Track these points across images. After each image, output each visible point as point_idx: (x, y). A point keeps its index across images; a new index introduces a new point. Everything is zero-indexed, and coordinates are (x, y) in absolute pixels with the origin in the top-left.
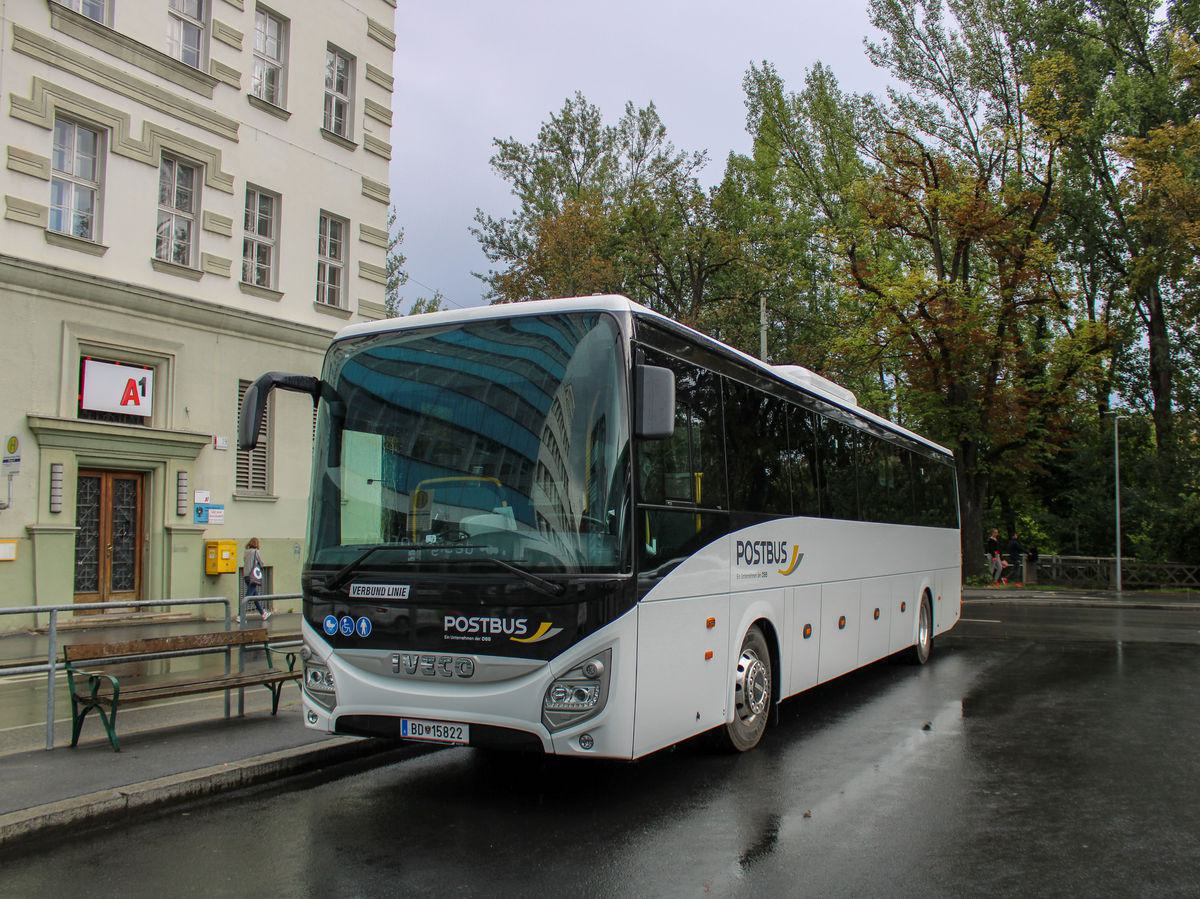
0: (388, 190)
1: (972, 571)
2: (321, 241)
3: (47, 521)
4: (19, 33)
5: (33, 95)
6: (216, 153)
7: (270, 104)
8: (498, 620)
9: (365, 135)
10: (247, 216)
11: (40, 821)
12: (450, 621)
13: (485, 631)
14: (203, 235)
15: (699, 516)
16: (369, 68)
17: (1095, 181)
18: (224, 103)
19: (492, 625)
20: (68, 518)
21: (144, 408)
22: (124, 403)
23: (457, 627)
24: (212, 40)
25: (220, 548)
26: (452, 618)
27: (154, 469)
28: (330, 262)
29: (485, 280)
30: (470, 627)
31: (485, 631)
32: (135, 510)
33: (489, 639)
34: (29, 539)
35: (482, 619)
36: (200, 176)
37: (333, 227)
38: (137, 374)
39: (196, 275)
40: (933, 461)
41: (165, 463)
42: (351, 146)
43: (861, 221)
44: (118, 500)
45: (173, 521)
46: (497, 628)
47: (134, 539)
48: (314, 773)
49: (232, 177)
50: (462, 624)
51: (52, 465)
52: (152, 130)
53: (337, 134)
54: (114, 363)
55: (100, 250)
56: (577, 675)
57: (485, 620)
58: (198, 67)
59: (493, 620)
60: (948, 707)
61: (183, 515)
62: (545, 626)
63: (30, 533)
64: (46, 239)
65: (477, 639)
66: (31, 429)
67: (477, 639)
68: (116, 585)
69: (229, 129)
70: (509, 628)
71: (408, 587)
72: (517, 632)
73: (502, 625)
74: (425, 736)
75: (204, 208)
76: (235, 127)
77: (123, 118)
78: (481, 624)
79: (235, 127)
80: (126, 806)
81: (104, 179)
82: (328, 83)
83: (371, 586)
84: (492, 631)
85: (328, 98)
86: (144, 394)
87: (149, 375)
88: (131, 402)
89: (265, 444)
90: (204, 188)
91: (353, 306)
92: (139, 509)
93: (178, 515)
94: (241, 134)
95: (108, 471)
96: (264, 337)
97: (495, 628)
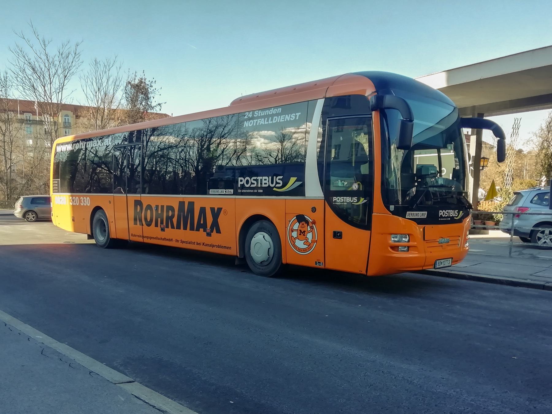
1: (304, 125)
8: (267, 178)
12: (335, 199)
13: (345, 201)
15: (330, 128)
19: (264, 182)
23: (337, 200)
26: (242, 178)
30: (252, 183)
31: (345, 201)
33: (346, 204)
35: (344, 198)
40: (421, 191)
46: (348, 200)
48: (446, 219)
50: (247, 182)
57: (345, 198)
60: (232, 173)
65: (343, 204)
67: (343, 204)
70: (352, 200)
72: (354, 201)
73: (350, 199)
78: (344, 199)
84: (347, 201)
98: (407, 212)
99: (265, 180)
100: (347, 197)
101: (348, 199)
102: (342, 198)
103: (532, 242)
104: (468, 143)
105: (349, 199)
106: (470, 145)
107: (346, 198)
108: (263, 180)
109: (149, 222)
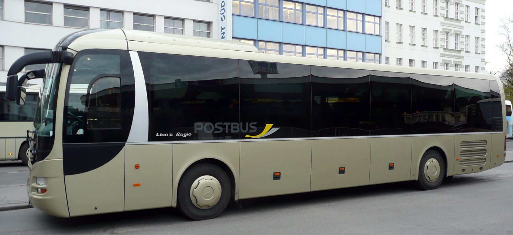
0: (485, 45)
11: (145, 230)
13: (227, 132)
17: (199, 102)
18: (463, 23)
19: (233, 127)
29: (502, 55)
31: (227, 132)
35: (225, 124)
43: (20, 75)
46: (236, 129)
57: (227, 124)
59: (233, 124)
69: (462, 57)
70: (244, 128)
73: (239, 127)
77: (451, 61)
78: (224, 127)
80: (172, 206)
82: (483, 40)
84: (233, 131)
97: (234, 129)
98: (194, 124)
99: (235, 125)
100: (231, 121)
101: (235, 127)
102: (218, 125)
103: (254, 69)
104: (95, 100)
105: (237, 127)
106: (261, 53)
107: (229, 124)
108: (232, 125)
109: (24, 104)
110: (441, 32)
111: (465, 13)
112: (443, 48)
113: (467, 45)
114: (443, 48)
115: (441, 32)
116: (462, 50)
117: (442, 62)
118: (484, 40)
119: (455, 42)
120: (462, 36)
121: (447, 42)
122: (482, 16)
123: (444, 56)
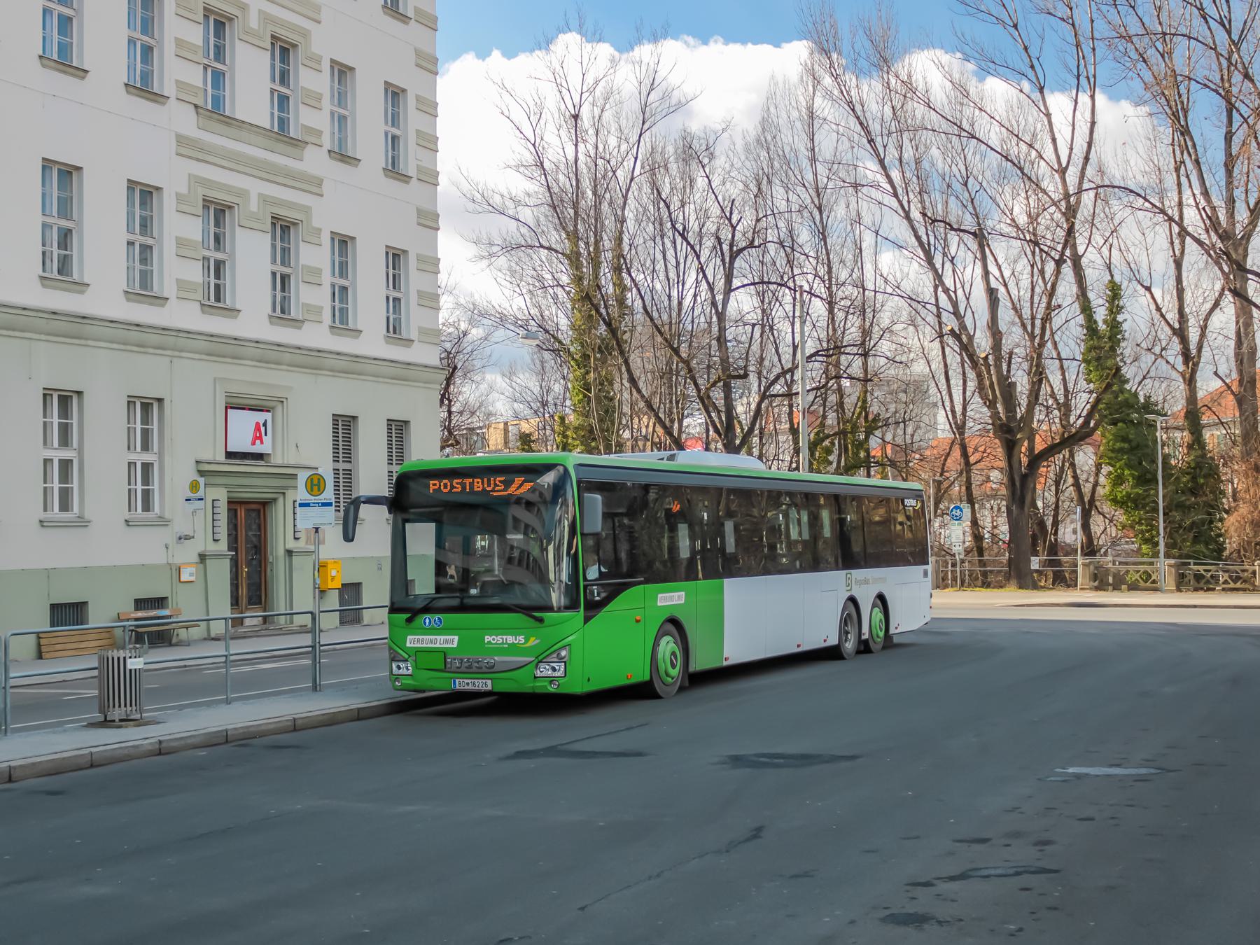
2: (130, 215)
3: (212, 548)
4: (181, 140)
5: (189, 191)
6: (307, 210)
7: (343, 156)
9: (417, 165)
10: (44, 195)
14: (302, 286)
16: (418, 98)
18: (315, 161)
20: (223, 546)
21: (264, 447)
22: (254, 443)
24: (301, 106)
25: (329, 567)
27: (275, 500)
28: (139, 239)
32: (260, 536)
34: (201, 563)
36: (232, 216)
37: (395, 257)
38: (261, 417)
39: (298, 323)
41: (284, 494)
42: (159, 98)
44: (248, 528)
45: (291, 544)
47: (260, 562)
49: (320, 230)
51: (213, 501)
52: (265, 200)
53: (394, 171)
54: (243, 409)
55: (233, 312)
56: (1177, 516)
57: (505, 637)
58: (72, 62)
61: (298, 539)
62: (532, 639)
63: (203, 557)
64: (202, 309)
66: (199, 471)
68: (250, 602)
69: (314, 185)
71: (456, 638)
74: (466, 687)
75: (302, 261)
76: (319, 182)
77: (243, 194)
78: (503, 639)
79: (319, 182)
81: (234, 247)
83: (425, 637)
85: (131, 42)
86: (266, 435)
87: (268, 416)
88: (258, 442)
89: (350, 470)
90: (301, 244)
91: (414, 335)
92: (263, 535)
93: (214, 540)
94: (326, 188)
95: (703, 490)
96: (224, 357)
110: (179, 198)
111: (327, 279)
112: (196, 106)
113: (344, 289)
114: (196, 106)
115: (179, 198)
116: (307, 316)
117: (184, 190)
118: (433, 304)
119: (267, 267)
120: (309, 58)
121: (219, 265)
122: (421, 294)
123: (200, 156)
